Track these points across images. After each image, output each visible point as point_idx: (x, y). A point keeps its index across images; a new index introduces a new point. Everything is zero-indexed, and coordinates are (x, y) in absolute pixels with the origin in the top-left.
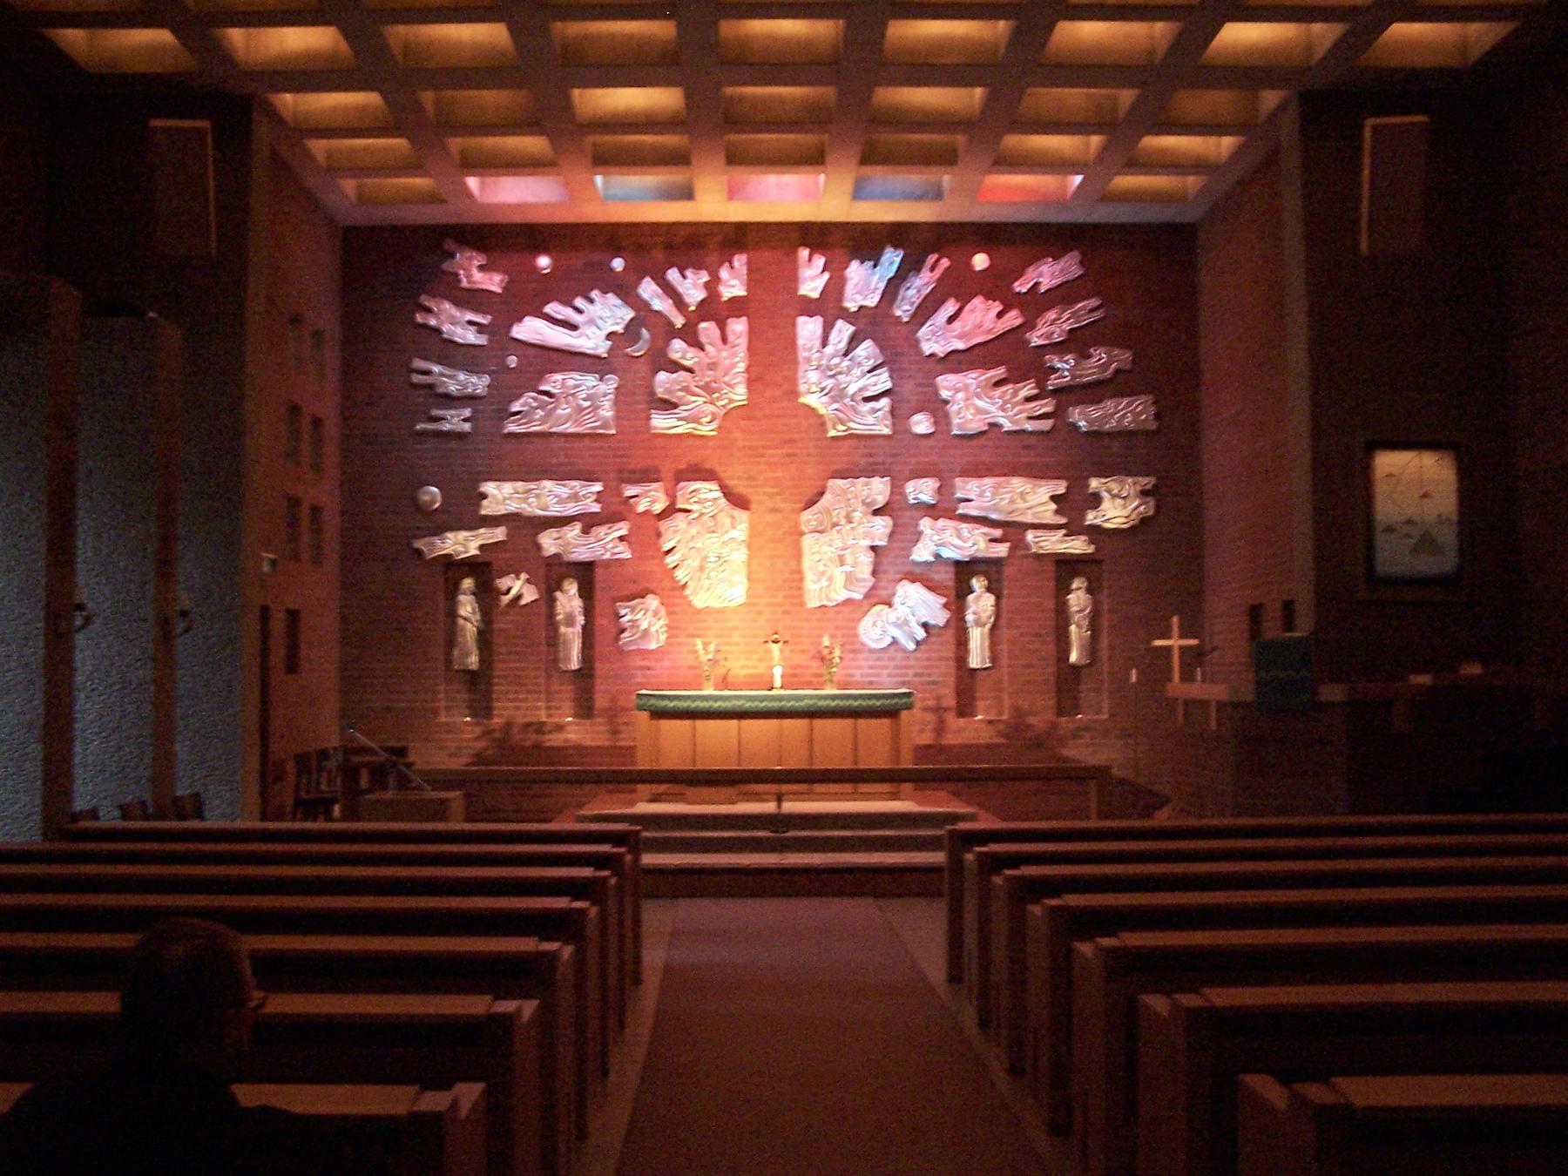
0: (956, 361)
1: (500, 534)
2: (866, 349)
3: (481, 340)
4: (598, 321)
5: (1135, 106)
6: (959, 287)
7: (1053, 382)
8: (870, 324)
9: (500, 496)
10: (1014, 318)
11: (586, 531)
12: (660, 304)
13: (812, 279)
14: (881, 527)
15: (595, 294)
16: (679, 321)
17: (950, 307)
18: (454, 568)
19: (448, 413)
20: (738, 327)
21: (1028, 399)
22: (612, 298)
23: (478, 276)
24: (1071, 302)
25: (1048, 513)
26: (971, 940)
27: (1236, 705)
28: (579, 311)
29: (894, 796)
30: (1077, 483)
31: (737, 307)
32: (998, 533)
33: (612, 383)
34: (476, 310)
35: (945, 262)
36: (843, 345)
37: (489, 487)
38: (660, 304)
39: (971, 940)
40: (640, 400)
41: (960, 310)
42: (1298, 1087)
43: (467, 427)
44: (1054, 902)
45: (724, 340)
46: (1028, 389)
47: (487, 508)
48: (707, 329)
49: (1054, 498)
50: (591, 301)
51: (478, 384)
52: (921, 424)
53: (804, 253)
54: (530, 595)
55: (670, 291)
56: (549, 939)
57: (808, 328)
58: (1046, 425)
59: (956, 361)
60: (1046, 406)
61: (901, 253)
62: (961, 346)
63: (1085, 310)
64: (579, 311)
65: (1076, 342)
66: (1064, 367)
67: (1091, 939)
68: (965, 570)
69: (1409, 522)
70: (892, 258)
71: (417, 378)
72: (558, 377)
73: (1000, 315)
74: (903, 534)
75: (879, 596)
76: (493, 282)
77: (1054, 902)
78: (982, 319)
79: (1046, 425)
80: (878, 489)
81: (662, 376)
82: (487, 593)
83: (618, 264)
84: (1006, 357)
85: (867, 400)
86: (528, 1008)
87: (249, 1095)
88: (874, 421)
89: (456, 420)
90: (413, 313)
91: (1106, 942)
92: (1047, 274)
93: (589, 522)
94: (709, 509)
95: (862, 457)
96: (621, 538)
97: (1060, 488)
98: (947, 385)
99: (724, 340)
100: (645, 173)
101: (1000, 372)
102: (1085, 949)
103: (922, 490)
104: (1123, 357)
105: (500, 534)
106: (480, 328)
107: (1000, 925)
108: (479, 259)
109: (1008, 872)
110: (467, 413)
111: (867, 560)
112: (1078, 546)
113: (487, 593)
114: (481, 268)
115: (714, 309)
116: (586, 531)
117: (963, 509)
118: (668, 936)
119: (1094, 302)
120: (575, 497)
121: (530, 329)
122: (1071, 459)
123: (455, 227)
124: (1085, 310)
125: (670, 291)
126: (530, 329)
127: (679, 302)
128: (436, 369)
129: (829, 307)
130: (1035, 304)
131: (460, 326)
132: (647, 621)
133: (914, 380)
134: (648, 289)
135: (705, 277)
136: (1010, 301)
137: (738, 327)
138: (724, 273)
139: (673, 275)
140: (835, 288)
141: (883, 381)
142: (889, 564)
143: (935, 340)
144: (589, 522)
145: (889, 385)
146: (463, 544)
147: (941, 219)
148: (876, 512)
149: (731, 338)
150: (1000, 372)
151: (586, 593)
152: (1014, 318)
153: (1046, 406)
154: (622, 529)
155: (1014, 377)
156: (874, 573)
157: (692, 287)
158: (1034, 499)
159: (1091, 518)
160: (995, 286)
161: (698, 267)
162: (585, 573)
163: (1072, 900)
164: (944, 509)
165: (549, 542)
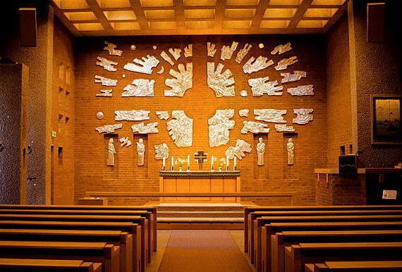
0: (255, 75)
1: (120, 126)
2: (228, 72)
3: (115, 70)
4: (149, 63)
5: (256, 13)
6: (254, 54)
7: (283, 81)
8: (228, 64)
9: (121, 115)
10: (271, 62)
11: (145, 125)
12: (168, 59)
13: (211, 52)
14: (231, 124)
15: (148, 56)
16: (173, 64)
17: (252, 59)
18: (108, 136)
19: (106, 91)
20: (190, 65)
21: (275, 86)
22: (153, 58)
23: (114, 51)
24: (288, 58)
25: (281, 119)
26: (250, 239)
27: (334, 175)
28: (143, 61)
29: (236, 202)
30: (290, 111)
31: (189, 60)
32: (266, 125)
33: (153, 81)
34: (113, 61)
35: (251, 46)
36: (220, 71)
37: (117, 112)
38: (168, 59)
39: (250, 239)
40: (161, 87)
41: (255, 60)
42: (316, 265)
43: (111, 95)
44: (280, 234)
45: (186, 69)
46: (276, 83)
47: (117, 118)
48: (181, 67)
49: (283, 115)
50: (147, 58)
51: (114, 82)
52: (244, 94)
53: (209, 44)
54: (129, 143)
55: (170, 55)
56: (125, 231)
57: (211, 66)
58: (280, 94)
59: (255, 75)
60: (281, 88)
61: (237, 43)
62: (256, 70)
63: (293, 60)
64: (143, 61)
65: (290, 69)
66: (287, 78)
67: (290, 246)
68: (256, 136)
69: (386, 121)
70: (235, 45)
71: (96, 81)
72: (137, 80)
73: (267, 62)
74: (239, 125)
75: (231, 143)
76: (119, 53)
77: (280, 234)
78: (260, 63)
79: (280, 94)
80: (231, 112)
81: (168, 80)
82: (117, 143)
83: (155, 47)
84: (270, 74)
85: (227, 86)
86: (116, 248)
87: (34, 9)
88: (229, 92)
89: (107, 93)
90: (95, 62)
91: (295, 246)
92: (281, 49)
93: (146, 122)
94: (182, 119)
95: (227, 103)
96: (156, 127)
97: (285, 112)
98: (252, 82)
99: (186, 69)
100: (127, 31)
101: (267, 78)
102: (289, 249)
103: (244, 112)
104: (304, 74)
105: (120, 126)
106: (115, 66)
107: (256, 232)
108: (115, 46)
109: (278, 233)
110: (111, 91)
111: (227, 133)
112: (291, 129)
113: (117, 143)
114: (115, 49)
115: (183, 60)
116: (145, 125)
117: (258, 118)
118: (163, 236)
119: (295, 57)
120: (143, 116)
121: (129, 67)
122: (286, 102)
123: (110, 37)
124: (293, 60)
125: (170, 55)
126: (129, 67)
127: (172, 58)
128: (102, 78)
129: (217, 59)
130: (277, 58)
131: (107, 65)
132: (163, 150)
133: (242, 80)
134: (163, 54)
135: (180, 51)
136: (270, 57)
137: (190, 65)
138: (186, 49)
139: (171, 50)
140: (219, 53)
141: (232, 81)
142: (235, 133)
143: (249, 68)
144: (146, 122)
145: (234, 82)
146: (109, 129)
147: (250, 33)
148: (230, 119)
149: (188, 69)
150: (267, 78)
151: (146, 144)
152: (271, 62)
153: (281, 88)
154: (156, 124)
155: (271, 80)
156: (230, 137)
157: (176, 54)
158: (275, 115)
159: (295, 121)
160: (266, 53)
161: (178, 48)
162: (145, 136)
163: (303, 245)
164: (251, 117)
165: (135, 128)
